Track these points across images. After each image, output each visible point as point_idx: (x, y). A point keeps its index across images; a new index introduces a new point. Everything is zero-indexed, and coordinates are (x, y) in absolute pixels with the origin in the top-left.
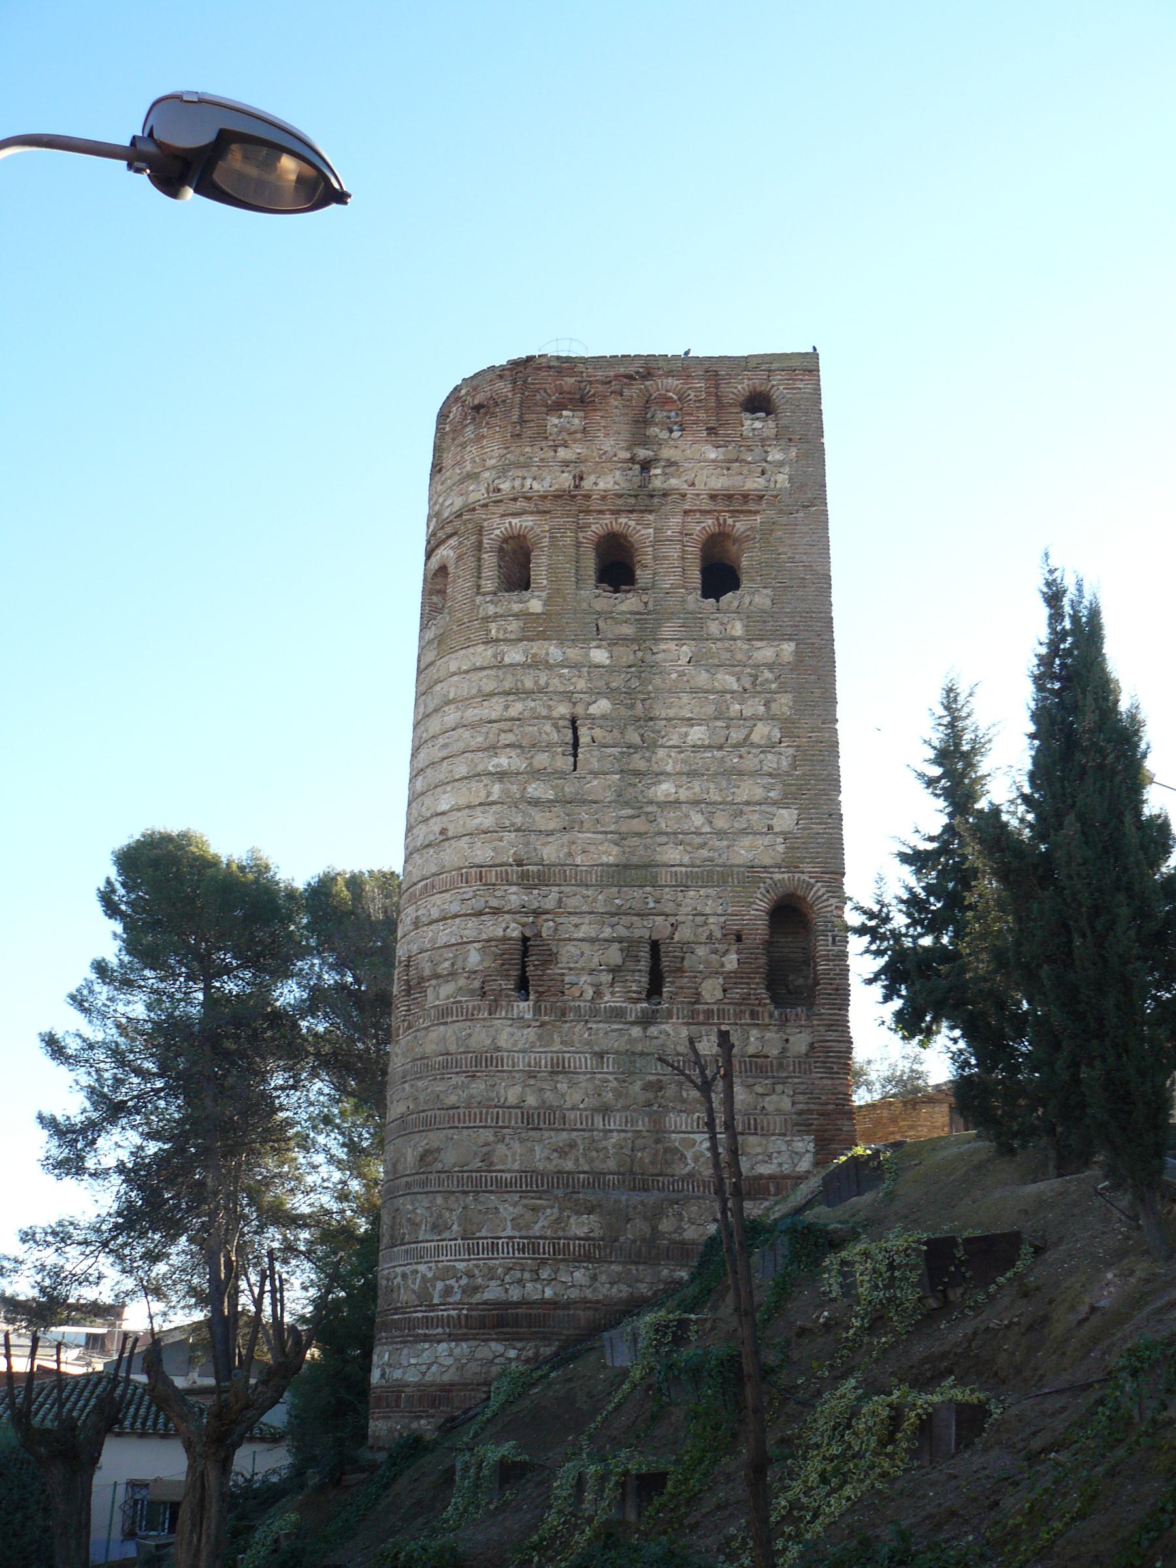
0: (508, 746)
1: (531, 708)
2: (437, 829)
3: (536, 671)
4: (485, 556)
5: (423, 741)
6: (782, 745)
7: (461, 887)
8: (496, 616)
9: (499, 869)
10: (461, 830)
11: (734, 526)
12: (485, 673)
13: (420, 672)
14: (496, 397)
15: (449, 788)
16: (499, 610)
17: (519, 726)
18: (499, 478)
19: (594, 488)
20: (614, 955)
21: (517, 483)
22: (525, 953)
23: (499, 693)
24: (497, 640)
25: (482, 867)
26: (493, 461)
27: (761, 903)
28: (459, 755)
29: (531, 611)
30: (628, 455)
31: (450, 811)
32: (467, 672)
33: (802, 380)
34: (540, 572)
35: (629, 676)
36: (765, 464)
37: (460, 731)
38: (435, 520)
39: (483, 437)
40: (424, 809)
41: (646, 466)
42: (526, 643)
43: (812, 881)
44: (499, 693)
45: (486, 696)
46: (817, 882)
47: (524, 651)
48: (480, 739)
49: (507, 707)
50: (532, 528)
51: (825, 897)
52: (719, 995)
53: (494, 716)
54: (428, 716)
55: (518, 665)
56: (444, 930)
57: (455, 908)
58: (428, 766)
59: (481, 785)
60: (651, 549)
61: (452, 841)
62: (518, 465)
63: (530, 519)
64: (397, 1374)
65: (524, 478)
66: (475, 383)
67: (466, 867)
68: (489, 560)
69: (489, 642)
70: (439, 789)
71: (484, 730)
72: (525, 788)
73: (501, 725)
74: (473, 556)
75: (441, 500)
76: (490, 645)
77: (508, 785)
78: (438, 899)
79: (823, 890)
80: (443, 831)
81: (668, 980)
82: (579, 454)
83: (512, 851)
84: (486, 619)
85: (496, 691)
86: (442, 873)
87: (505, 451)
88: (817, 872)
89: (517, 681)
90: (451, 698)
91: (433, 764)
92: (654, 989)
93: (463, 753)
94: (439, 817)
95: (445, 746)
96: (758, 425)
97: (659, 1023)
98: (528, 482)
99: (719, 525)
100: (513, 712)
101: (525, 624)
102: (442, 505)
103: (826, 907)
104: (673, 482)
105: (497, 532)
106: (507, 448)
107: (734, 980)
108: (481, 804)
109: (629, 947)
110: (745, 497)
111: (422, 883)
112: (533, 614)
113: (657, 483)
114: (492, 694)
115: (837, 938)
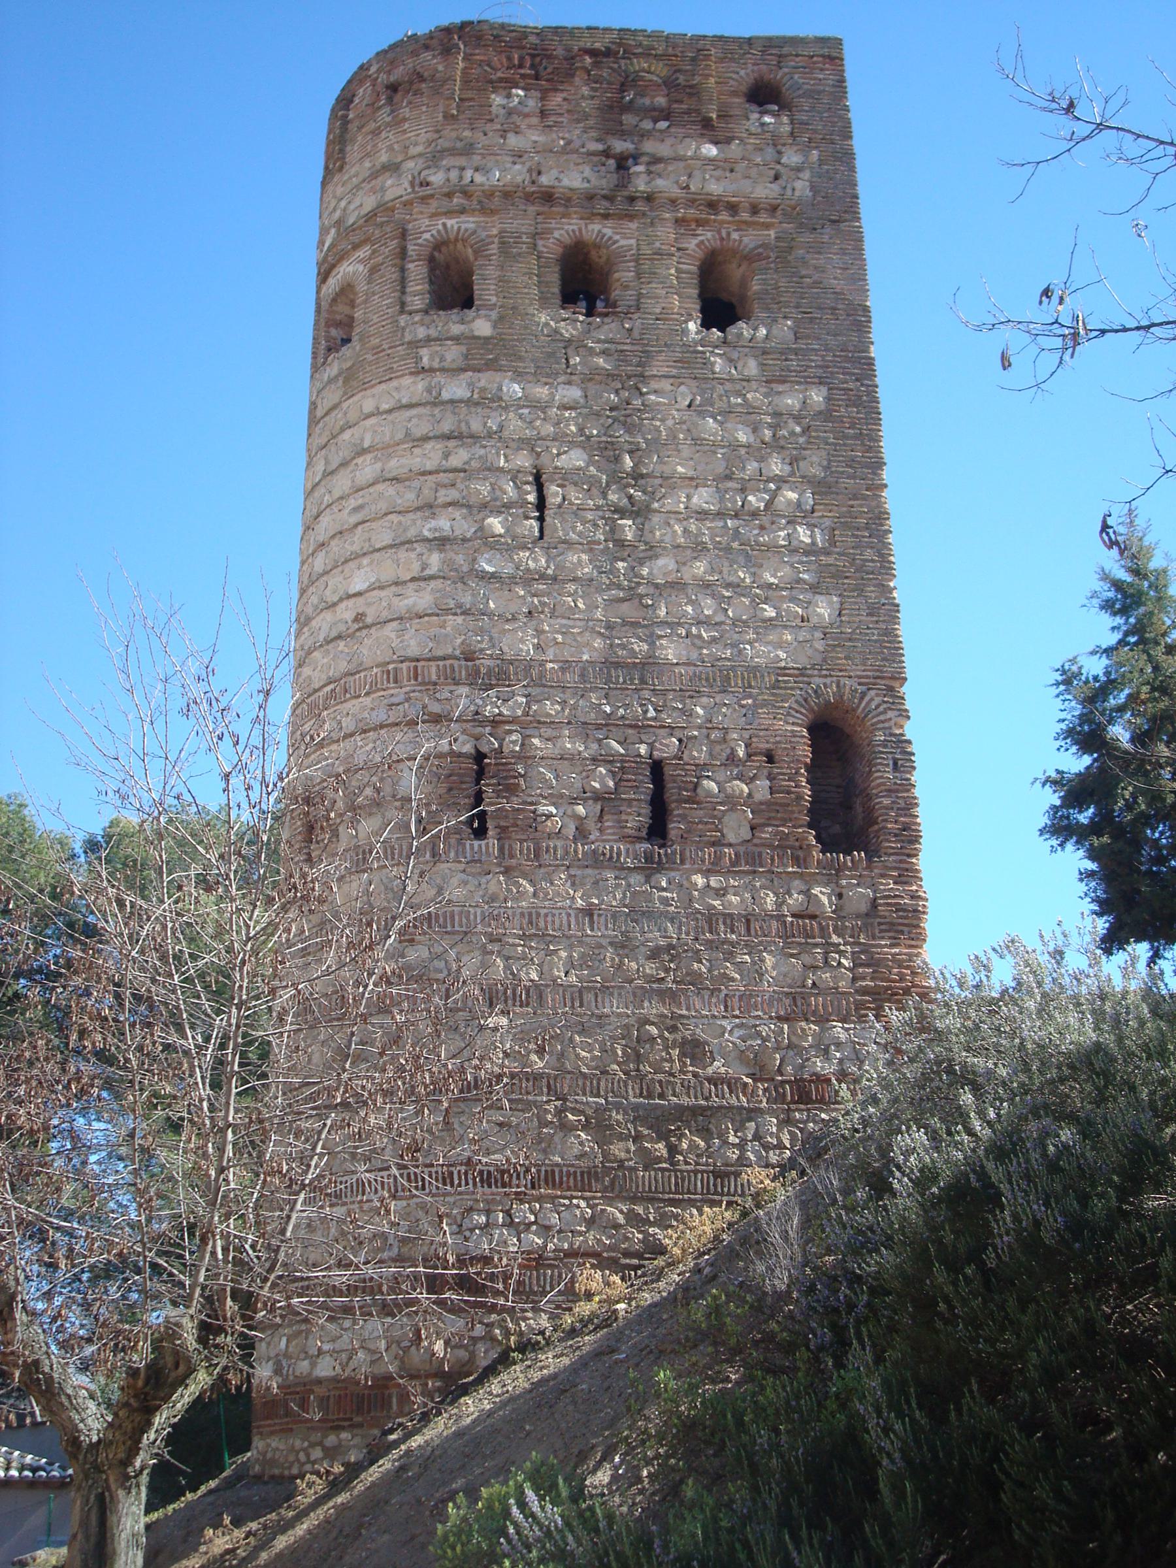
0: (450, 504)
1: (481, 457)
2: (349, 616)
3: (486, 410)
4: (411, 266)
5: (323, 506)
6: (815, 514)
7: (388, 688)
8: (428, 340)
9: (441, 663)
10: (385, 615)
11: (741, 241)
12: (414, 412)
13: (313, 421)
14: (421, 70)
15: (365, 561)
16: (433, 333)
17: (464, 479)
18: (429, 167)
19: (557, 184)
20: (602, 779)
21: (454, 175)
22: (480, 774)
23: (436, 437)
24: (432, 370)
25: (418, 660)
26: (420, 149)
27: (798, 715)
28: (382, 518)
29: (476, 333)
30: (600, 147)
31: (367, 591)
32: (390, 411)
33: (822, 70)
34: (486, 288)
35: (610, 421)
36: (778, 167)
37: (380, 487)
38: (333, 231)
39: (405, 120)
40: (328, 592)
41: (623, 163)
42: (470, 373)
43: (864, 688)
44: (436, 437)
45: (418, 440)
46: (869, 689)
47: (469, 385)
48: (411, 496)
49: (446, 456)
50: (474, 232)
51: (881, 709)
52: (746, 833)
53: (429, 466)
54: (332, 473)
55: (461, 401)
56: (362, 747)
57: (381, 716)
58: (333, 537)
59: (413, 555)
60: (632, 264)
61: (373, 630)
62: (452, 152)
63: (471, 219)
64: (304, 1366)
65: (463, 169)
66: (390, 55)
67: (393, 662)
68: (417, 271)
69: (418, 373)
70: (352, 565)
71: (416, 484)
72: (474, 560)
73: (443, 477)
74: (393, 266)
75: (343, 204)
76: (421, 376)
77: (451, 555)
78: (352, 706)
79: (877, 700)
80: (359, 617)
81: (676, 812)
82: (536, 142)
83: (459, 641)
84: (415, 344)
85: (431, 434)
86: (359, 672)
87: (436, 136)
88: (868, 677)
89: (460, 421)
90: (366, 445)
91: (341, 533)
92: (657, 830)
93: (386, 514)
94: (353, 600)
95: (356, 509)
96: (768, 119)
97: (667, 869)
98: (468, 174)
99: (722, 239)
100: (455, 461)
101: (468, 350)
102: (345, 210)
103: (883, 722)
104: (660, 183)
105: (427, 236)
106: (438, 131)
107: (767, 815)
108: (413, 579)
109: (621, 768)
110: (755, 209)
111: (329, 688)
112: (479, 338)
113: (641, 185)
114: (426, 439)
115: (900, 762)
